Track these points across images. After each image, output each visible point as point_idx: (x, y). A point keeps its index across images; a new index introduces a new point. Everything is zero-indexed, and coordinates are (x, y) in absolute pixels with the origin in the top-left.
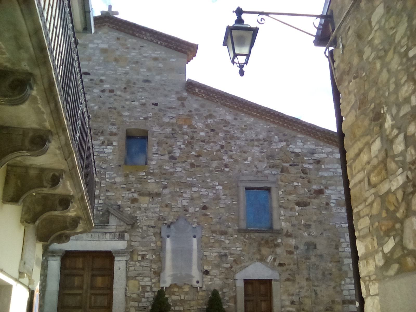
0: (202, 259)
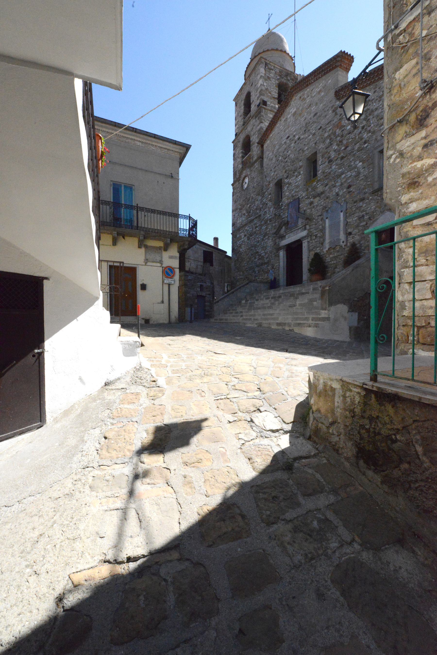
0: (347, 224)
